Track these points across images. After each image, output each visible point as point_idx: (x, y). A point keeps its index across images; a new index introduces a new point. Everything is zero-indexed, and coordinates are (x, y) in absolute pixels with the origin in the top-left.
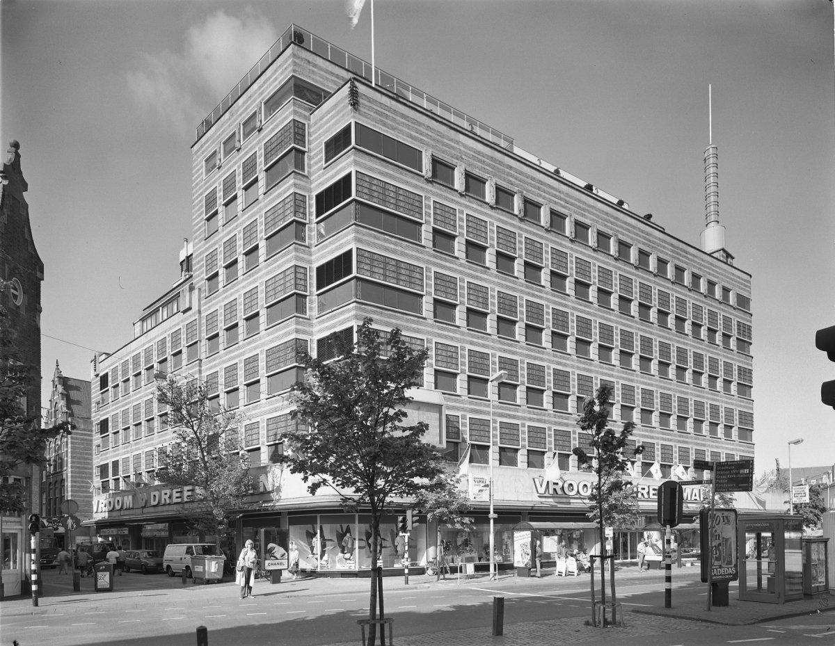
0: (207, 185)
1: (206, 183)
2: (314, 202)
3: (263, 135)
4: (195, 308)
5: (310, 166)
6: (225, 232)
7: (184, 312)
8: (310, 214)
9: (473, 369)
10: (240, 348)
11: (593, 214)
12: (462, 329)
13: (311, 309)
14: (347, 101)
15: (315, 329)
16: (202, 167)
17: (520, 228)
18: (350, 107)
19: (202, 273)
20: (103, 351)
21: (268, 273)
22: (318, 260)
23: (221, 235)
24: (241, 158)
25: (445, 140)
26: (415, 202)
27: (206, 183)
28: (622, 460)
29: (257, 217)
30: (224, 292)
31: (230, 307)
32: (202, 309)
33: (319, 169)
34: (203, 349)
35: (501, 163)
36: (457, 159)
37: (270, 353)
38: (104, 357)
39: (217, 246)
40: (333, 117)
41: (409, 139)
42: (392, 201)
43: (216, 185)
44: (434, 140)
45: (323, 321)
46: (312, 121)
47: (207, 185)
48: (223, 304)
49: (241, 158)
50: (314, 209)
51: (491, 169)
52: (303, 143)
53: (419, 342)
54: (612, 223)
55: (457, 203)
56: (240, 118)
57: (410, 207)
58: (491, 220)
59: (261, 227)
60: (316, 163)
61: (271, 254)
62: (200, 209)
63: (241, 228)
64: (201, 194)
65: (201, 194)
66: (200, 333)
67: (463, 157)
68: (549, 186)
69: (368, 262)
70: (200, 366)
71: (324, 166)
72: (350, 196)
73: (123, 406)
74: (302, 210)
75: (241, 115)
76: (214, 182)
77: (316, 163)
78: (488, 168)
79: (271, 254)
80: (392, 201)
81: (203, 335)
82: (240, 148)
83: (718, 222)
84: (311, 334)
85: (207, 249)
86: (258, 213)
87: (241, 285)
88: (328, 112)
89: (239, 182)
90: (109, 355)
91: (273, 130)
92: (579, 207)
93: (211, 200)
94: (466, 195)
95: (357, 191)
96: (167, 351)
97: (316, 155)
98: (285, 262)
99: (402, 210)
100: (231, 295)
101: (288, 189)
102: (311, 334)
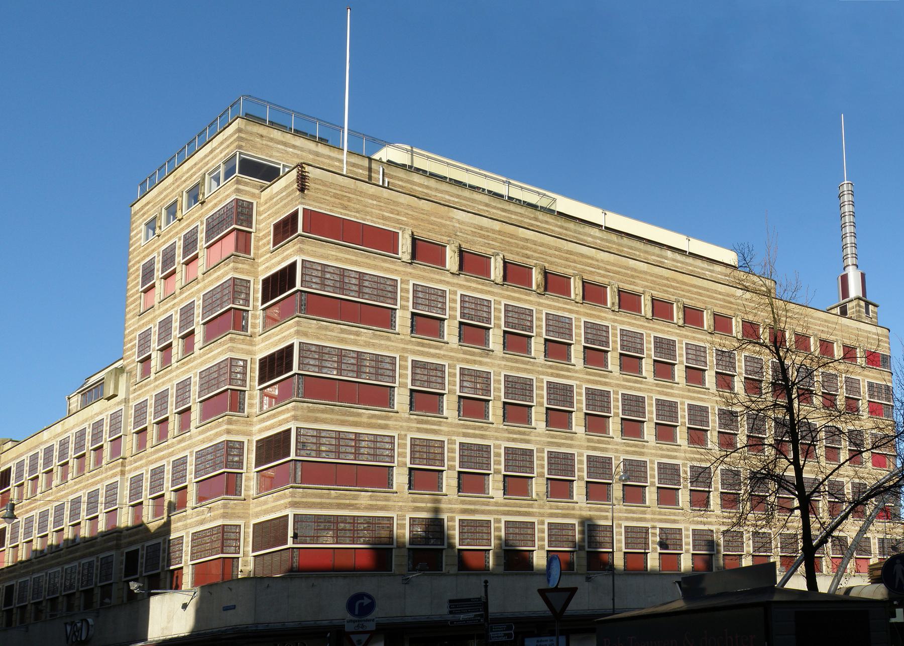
0: (145, 253)
1: (144, 251)
2: (260, 287)
3: (206, 208)
4: (122, 395)
5: (257, 248)
6: (161, 310)
7: (109, 399)
8: (255, 299)
9: (660, 417)
10: (168, 447)
11: (647, 280)
12: (449, 420)
13: (251, 405)
14: (295, 186)
15: (255, 428)
16: (141, 231)
17: (539, 304)
18: (298, 193)
19: (133, 354)
20: (9, 438)
21: (201, 364)
22: (261, 351)
23: (157, 312)
24: (182, 229)
25: (433, 218)
26: (387, 288)
27: (144, 251)
28: (363, 599)
29: (195, 298)
30: (200, 356)
31: (162, 398)
32: (131, 396)
33: (267, 252)
34: (128, 446)
35: (512, 236)
36: (450, 237)
37: (200, 455)
38: (10, 445)
39: (152, 325)
40: (282, 199)
41: (381, 221)
42: (354, 288)
43: (155, 254)
44: (416, 219)
45: (263, 420)
46: (263, 200)
47: (145, 253)
48: (176, 382)
49: (182, 229)
50: (259, 295)
51: (498, 244)
52: (249, 224)
53: (387, 440)
54: (674, 288)
55: (448, 283)
56: (183, 186)
57: (380, 293)
58: (496, 298)
59: (198, 311)
60: (264, 245)
61: (210, 337)
62: (136, 278)
63: (178, 308)
64: (139, 262)
65: (139, 262)
66: (126, 427)
67: (458, 234)
68: (582, 255)
69: (317, 356)
70: (123, 465)
71: (272, 249)
72: (294, 286)
73: (27, 512)
74: (243, 296)
75: (185, 181)
76: (153, 251)
77: (264, 245)
78: (493, 243)
79: (210, 337)
80: (354, 288)
81: (129, 428)
82: (182, 218)
83: (857, 266)
84: (250, 434)
85: (140, 327)
86: (196, 295)
87: (174, 374)
88: (278, 193)
89: (179, 256)
90: (18, 443)
91: (216, 205)
92: (626, 275)
93: (148, 273)
94: (460, 274)
95: (302, 281)
96: (148, 419)
97: (265, 236)
98: (220, 354)
99: (367, 296)
100: (163, 383)
101: (227, 273)
102: (250, 434)
